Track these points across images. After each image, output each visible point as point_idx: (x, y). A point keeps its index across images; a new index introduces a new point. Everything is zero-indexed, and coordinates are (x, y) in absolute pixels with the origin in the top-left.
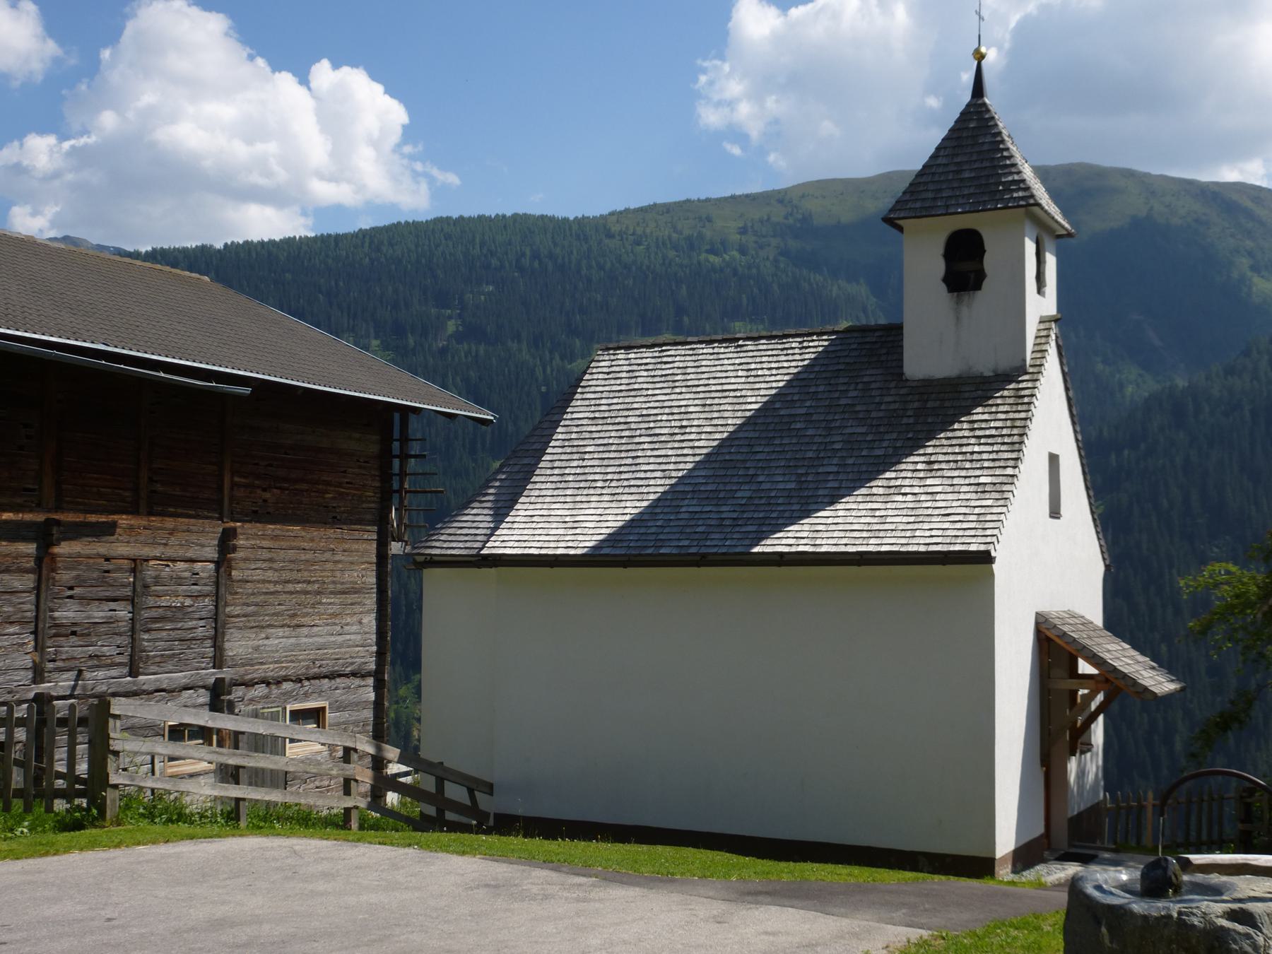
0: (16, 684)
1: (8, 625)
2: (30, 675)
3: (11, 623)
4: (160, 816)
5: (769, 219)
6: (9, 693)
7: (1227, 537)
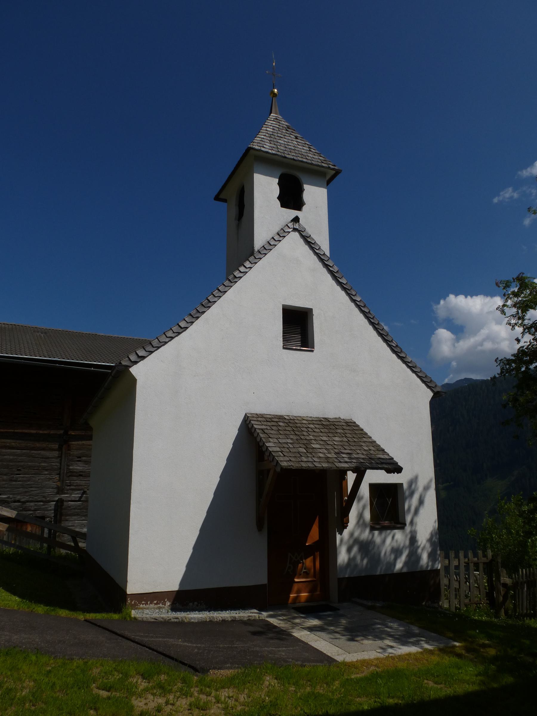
0: (47, 494)
1: (44, 471)
2: (56, 491)
3: (46, 470)
4: (175, 693)
5: (384, 671)
6: (43, 497)
7: (446, 606)
